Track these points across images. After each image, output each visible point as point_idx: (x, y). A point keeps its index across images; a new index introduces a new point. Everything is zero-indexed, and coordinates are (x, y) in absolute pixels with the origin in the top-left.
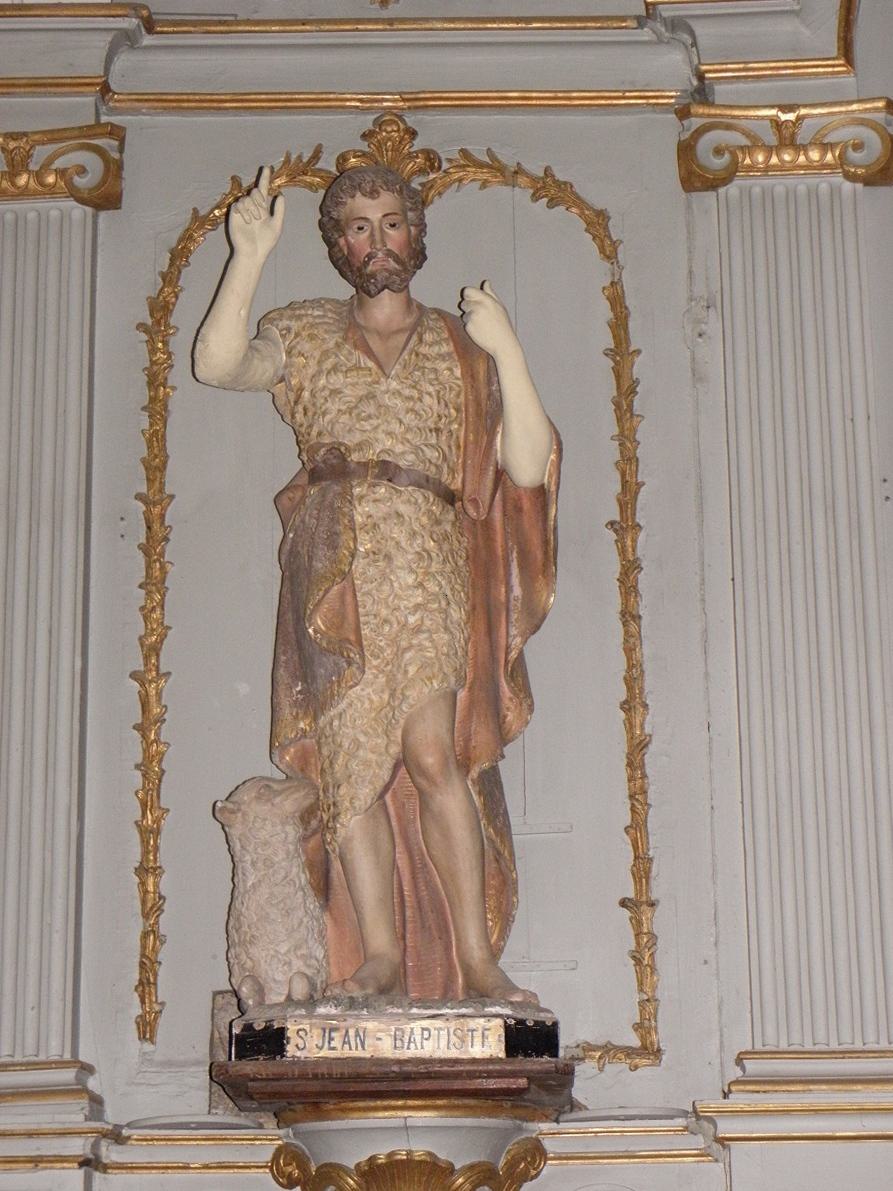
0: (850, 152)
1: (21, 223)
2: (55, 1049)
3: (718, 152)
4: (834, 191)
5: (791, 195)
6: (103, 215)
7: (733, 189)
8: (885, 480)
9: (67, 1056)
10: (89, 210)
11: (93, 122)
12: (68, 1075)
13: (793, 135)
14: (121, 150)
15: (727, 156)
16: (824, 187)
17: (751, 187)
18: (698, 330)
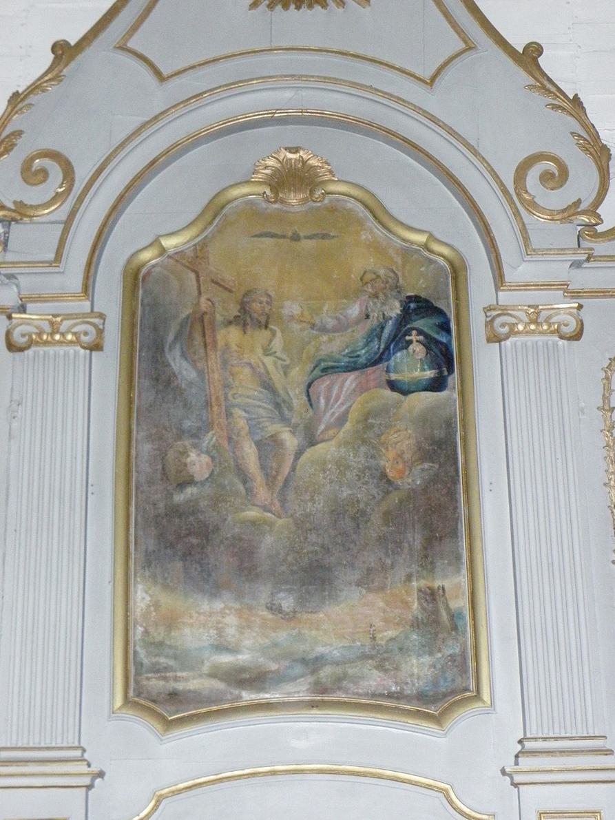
0: (563, 327)
1: (47, 355)
2: (71, 740)
3: (503, 325)
4: (555, 345)
5: (525, 345)
6: (94, 353)
7: (30, 352)
8: (491, 484)
9: (76, 744)
10: (88, 351)
11: (89, 311)
12: (78, 753)
13: (58, 328)
14: (104, 324)
15: (27, 337)
16: (72, 352)
17: (537, 342)
18: (13, 415)
